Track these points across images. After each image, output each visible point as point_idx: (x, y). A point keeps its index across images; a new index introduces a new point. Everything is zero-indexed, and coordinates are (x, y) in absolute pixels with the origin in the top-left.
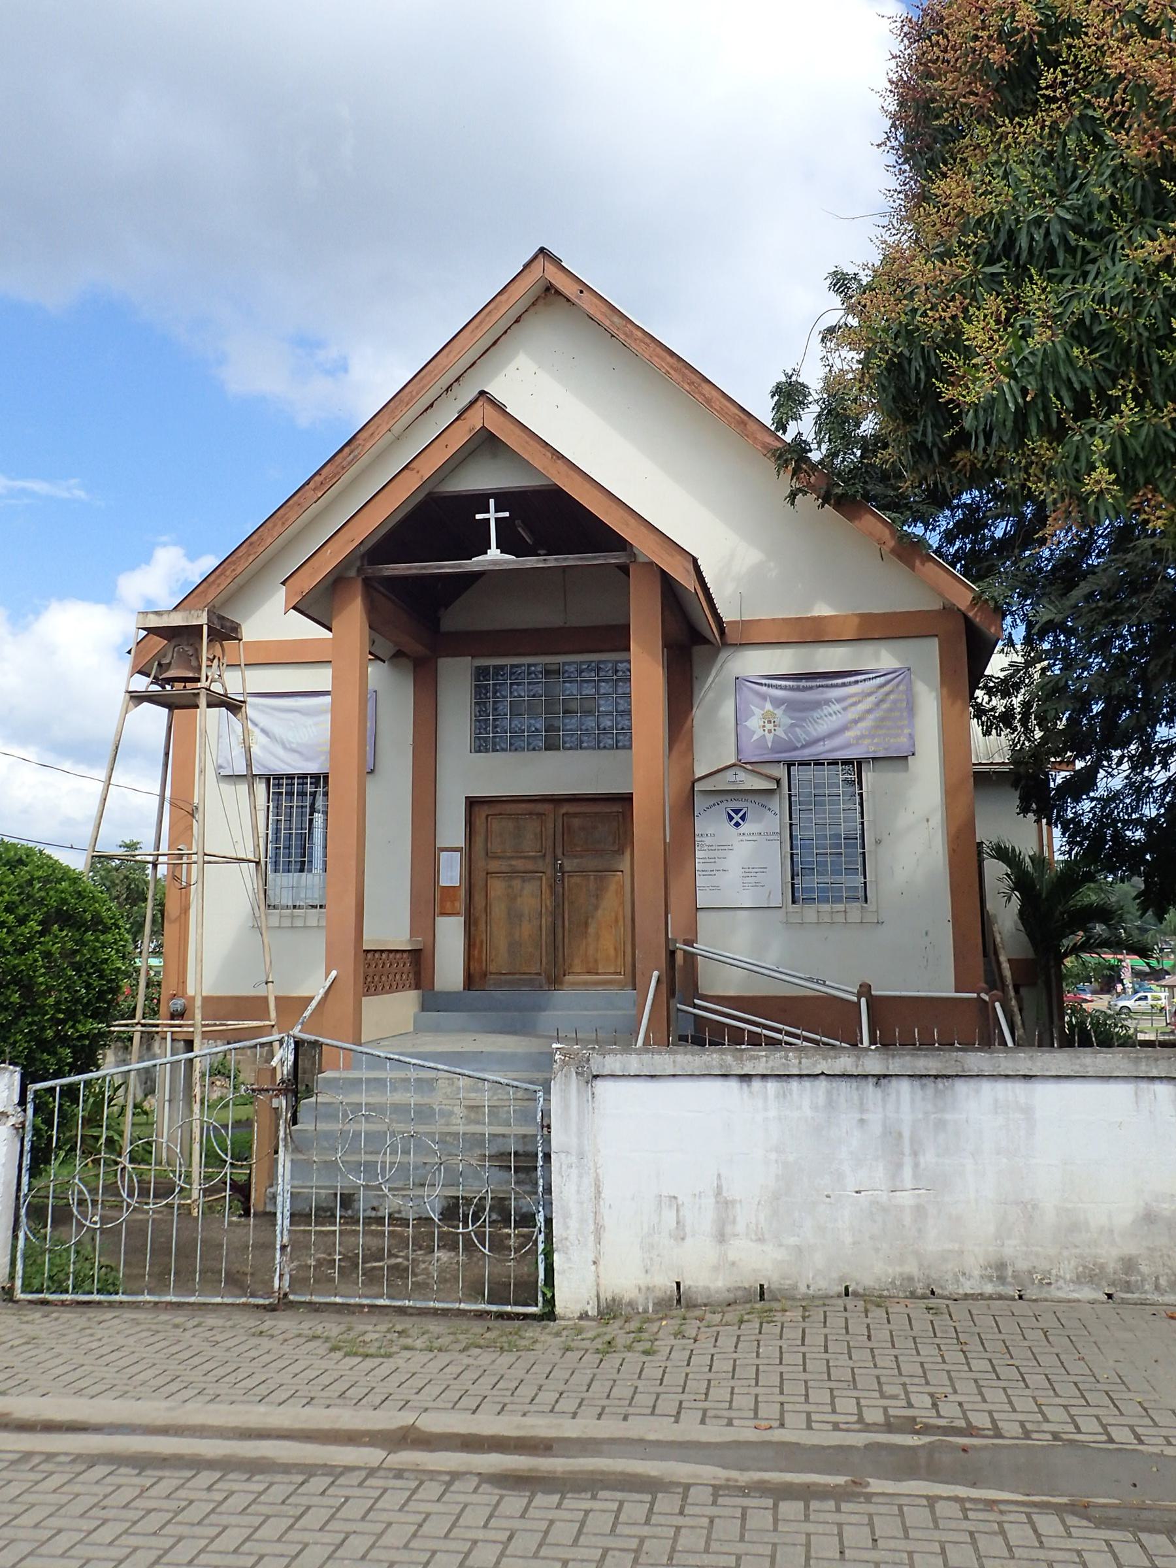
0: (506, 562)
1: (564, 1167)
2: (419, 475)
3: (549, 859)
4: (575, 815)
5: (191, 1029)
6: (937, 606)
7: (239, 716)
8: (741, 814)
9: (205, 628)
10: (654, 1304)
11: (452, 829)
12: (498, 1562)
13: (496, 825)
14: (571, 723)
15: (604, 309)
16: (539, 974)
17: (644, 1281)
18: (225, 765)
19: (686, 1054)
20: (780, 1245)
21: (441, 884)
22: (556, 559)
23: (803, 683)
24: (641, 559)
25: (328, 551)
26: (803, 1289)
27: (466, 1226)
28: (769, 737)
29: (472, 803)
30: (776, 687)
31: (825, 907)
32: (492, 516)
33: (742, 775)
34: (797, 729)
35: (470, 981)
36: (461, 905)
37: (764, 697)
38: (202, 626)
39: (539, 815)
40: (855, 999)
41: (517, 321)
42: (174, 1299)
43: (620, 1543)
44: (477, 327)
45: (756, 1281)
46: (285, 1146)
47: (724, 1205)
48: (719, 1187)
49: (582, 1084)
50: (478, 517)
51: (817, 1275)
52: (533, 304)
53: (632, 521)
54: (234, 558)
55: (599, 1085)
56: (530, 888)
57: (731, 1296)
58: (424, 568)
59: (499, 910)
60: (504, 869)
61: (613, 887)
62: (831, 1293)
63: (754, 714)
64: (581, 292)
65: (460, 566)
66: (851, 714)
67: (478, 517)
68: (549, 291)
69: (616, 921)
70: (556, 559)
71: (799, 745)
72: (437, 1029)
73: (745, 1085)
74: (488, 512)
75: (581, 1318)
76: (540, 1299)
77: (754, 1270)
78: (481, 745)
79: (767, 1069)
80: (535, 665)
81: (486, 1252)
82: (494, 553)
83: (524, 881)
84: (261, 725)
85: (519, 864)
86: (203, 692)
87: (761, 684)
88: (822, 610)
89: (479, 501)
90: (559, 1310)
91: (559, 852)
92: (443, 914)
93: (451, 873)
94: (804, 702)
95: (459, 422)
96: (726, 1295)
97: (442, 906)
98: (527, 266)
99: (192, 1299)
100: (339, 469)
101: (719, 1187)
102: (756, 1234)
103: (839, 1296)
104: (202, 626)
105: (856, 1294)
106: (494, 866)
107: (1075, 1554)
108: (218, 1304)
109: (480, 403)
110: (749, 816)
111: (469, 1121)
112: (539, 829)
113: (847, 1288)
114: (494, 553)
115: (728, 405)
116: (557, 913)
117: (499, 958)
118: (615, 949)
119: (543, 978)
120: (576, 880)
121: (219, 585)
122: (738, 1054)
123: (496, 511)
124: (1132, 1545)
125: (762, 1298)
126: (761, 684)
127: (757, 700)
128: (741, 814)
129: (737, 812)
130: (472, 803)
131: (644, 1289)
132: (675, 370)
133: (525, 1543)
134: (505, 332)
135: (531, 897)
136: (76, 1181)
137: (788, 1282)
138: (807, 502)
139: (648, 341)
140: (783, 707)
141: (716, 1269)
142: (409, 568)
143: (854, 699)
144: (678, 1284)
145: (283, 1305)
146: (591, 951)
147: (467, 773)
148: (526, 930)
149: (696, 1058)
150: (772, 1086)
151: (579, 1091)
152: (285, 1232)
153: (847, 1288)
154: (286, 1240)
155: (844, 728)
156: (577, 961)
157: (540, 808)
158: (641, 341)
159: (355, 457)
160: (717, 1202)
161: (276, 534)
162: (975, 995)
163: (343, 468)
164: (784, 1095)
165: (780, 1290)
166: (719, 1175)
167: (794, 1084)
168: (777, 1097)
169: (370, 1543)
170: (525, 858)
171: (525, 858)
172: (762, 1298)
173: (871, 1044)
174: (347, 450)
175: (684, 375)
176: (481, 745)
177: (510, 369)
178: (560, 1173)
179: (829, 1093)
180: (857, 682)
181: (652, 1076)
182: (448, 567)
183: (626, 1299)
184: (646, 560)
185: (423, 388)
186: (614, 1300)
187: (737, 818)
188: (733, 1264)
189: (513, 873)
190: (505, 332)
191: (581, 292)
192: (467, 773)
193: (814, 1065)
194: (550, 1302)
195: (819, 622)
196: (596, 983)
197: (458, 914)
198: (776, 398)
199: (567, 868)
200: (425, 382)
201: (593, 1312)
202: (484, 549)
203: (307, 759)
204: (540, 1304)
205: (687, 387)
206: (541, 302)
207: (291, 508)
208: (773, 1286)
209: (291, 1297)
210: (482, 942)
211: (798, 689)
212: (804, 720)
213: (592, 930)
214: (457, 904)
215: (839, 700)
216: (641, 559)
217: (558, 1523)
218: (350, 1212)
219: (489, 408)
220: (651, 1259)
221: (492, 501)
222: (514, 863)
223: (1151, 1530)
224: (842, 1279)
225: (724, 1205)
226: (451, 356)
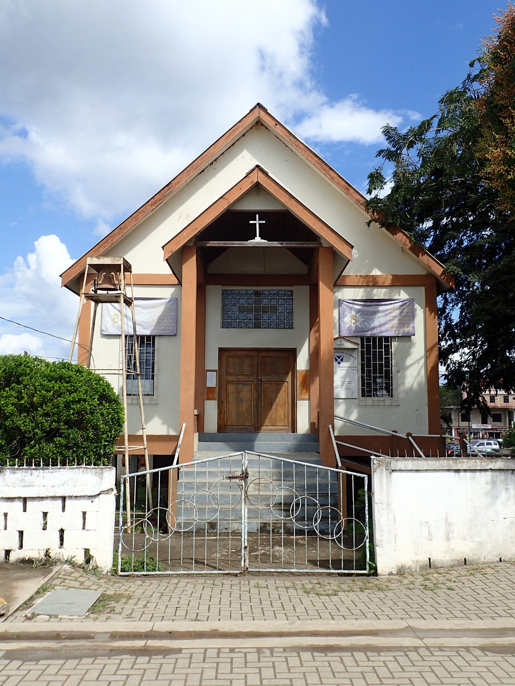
0: (264, 243)
1: (381, 510)
2: (227, 202)
3: (255, 376)
4: (267, 357)
5: (123, 450)
6: (424, 273)
7: (131, 307)
8: (341, 358)
9: (122, 266)
10: (420, 568)
11: (212, 361)
12: (140, 684)
13: (231, 361)
14: (265, 317)
15: (286, 133)
16: (251, 426)
17: (415, 558)
18: (105, 330)
19: (432, 460)
20: (473, 541)
21: (208, 386)
22: (286, 243)
23: (368, 303)
24: (325, 245)
25: (184, 233)
26: (483, 559)
27: (332, 536)
28: (353, 326)
29: (221, 350)
30: (357, 304)
31: (376, 399)
32: (257, 222)
33: (344, 342)
34: (366, 323)
35: (220, 429)
36: (216, 395)
37: (351, 308)
38: (120, 265)
39: (251, 356)
40: (406, 437)
41: (243, 136)
42: (195, 572)
43: (183, 671)
44: (228, 137)
45: (463, 557)
46: (245, 503)
47: (449, 525)
48: (447, 518)
49: (389, 473)
50: (251, 222)
51: (488, 554)
52: (251, 128)
53: (325, 228)
54: (112, 234)
55: (394, 474)
56: (246, 388)
57: (453, 563)
58: (226, 244)
59: (232, 398)
60: (235, 380)
61: (283, 389)
62: (494, 561)
63: (346, 315)
64: (276, 125)
65: (242, 244)
66: (388, 318)
67: (251, 222)
68: (259, 124)
69: (285, 403)
70: (286, 243)
71: (366, 330)
72: (208, 449)
73: (457, 474)
75: (389, 575)
76: (368, 567)
77: (462, 552)
78: (225, 325)
79: (467, 467)
80: (249, 290)
81: (342, 547)
82: (258, 239)
83: (243, 385)
85: (241, 378)
86: (122, 296)
87: (350, 303)
88: (376, 272)
89: (252, 215)
90: (379, 571)
91: (259, 373)
92: (208, 399)
93: (212, 381)
94: (368, 311)
95: (246, 178)
96: (450, 563)
97: (208, 396)
98: (251, 111)
99: (204, 572)
100: (163, 196)
101: (447, 518)
102: (462, 537)
103: (497, 562)
104: (120, 265)
105: (505, 561)
106: (230, 378)
108: (216, 574)
109: (256, 170)
110: (344, 360)
112: (250, 363)
113: (500, 559)
114: (258, 239)
115: (341, 180)
116: (258, 400)
117: (232, 418)
118: (284, 415)
119: (252, 428)
120: (267, 385)
122: (455, 461)
123: (259, 220)
124: (67, 662)
125: (465, 564)
126: (350, 303)
127: (348, 310)
128: (341, 358)
129: (339, 357)
130: (221, 350)
131: (415, 561)
132: (318, 163)
133: (151, 674)
134: (238, 140)
135: (247, 392)
136: (146, 519)
137: (477, 557)
138: (375, 225)
139: (306, 149)
140: (360, 313)
141: (446, 552)
142: (219, 244)
143: (390, 311)
144: (430, 559)
145: (245, 572)
146: (273, 416)
147: (219, 337)
148: (245, 406)
149: (437, 462)
150: (468, 474)
151: (387, 477)
152: (246, 541)
153: (500, 559)
154: (246, 544)
155: (385, 323)
156: (267, 420)
157: (251, 353)
158: (303, 149)
159: (171, 191)
160: (446, 524)
161: (132, 225)
162: (439, 436)
163: (165, 196)
164: (474, 478)
165: (473, 560)
166: (446, 512)
167: (478, 474)
168: (471, 479)
169: (204, 675)
170: (244, 375)
171: (244, 375)
172: (465, 564)
173: (116, 456)
174: (167, 188)
175: (322, 166)
176: (225, 325)
177: (240, 157)
178: (379, 512)
179: (492, 476)
180: (391, 304)
181: (417, 470)
182: (237, 244)
183: (407, 566)
185: (203, 162)
186: (402, 567)
187: (339, 360)
188: (453, 550)
189: (239, 382)
190: (238, 140)
191: (276, 125)
192: (219, 337)
193: (487, 465)
194: (376, 569)
195: (374, 277)
196: (276, 430)
197: (215, 399)
198: (369, 179)
199: (263, 380)
200: (204, 159)
201: (395, 572)
202: (254, 237)
203: (145, 329)
204: (368, 569)
205: (323, 171)
206: (254, 128)
207: (140, 213)
208: (470, 559)
209: (250, 570)
210: (225, 412)
211: (366, 306)
212: (368, 319)
213: (274, 407)
214: (215, 395)
215: (384, 311)
216: (325, 245)
217: (164, 665)
218: (215, 530)
219: (260, 174)
220: (418, 548)
221: (257, 216)
222: (239, 377)
223: (486, 651)
224: (499, 555)
225: (449, 525)
226: (216, 149)
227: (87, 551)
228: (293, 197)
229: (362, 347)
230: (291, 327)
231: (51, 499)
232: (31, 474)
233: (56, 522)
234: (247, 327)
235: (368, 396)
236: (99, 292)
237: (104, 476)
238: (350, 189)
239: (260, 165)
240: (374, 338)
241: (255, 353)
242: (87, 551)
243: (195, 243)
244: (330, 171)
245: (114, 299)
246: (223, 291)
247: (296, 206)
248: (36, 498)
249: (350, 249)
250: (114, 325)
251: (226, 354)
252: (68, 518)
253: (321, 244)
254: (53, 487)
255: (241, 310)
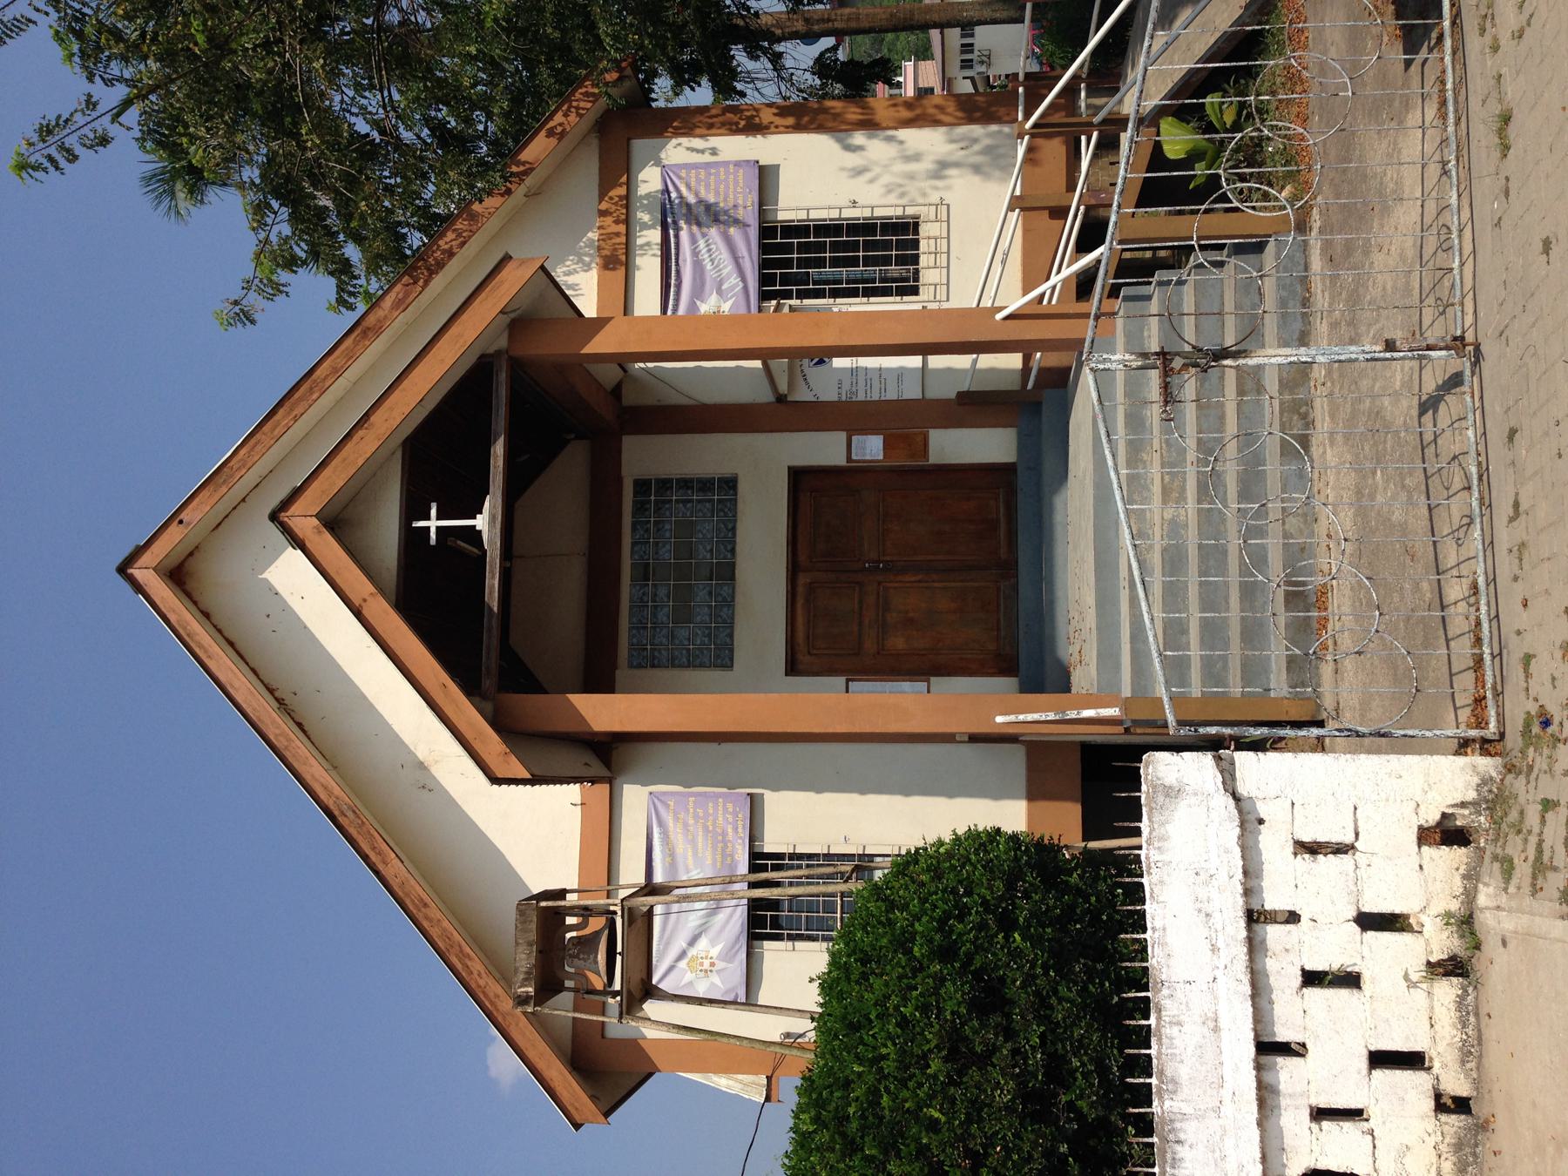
6: (594, 142)
24: (503, 343)
30: (677, 300)
64: (181, 522)
74: (428, 528)
82: (480, 522)
84: (684, 945)
89: (413, 540)
107: (1549, 816)
111: (1182, 498)
114: (480, 522)
121: (497, 996)
139: (253, 441)
175: (301, 399)
184: (506, 335)
191: (181, 522)
202: (473, 535)
205: (315, 396)
222: (866, 622)
227: (1425, 836)
228: (367, 415)
229: (788, 295)
230: (730, 484)
231: (1258, 959)
232: (1179, 1024)
233: (1335, 945)
234: (729, 602)
235: (916, 279)
236: (617, 986)
237: (1174, 783)
238: (365, 324)
239: (268, 511)
240: (764, 264)
241: (803, 579)
242: (1425, 836)
243: (484, 697)
244: (314, 376)
245: (640, 923)
246: (631, 666)
247: (391, 409)
248: (1254, 1005)
249: (510, 266)
250: (718, 972)
251: (804, 658)
252: (1321, 899)
253: (498, 353)
254: (1214, 949)
255: (683, 614)
